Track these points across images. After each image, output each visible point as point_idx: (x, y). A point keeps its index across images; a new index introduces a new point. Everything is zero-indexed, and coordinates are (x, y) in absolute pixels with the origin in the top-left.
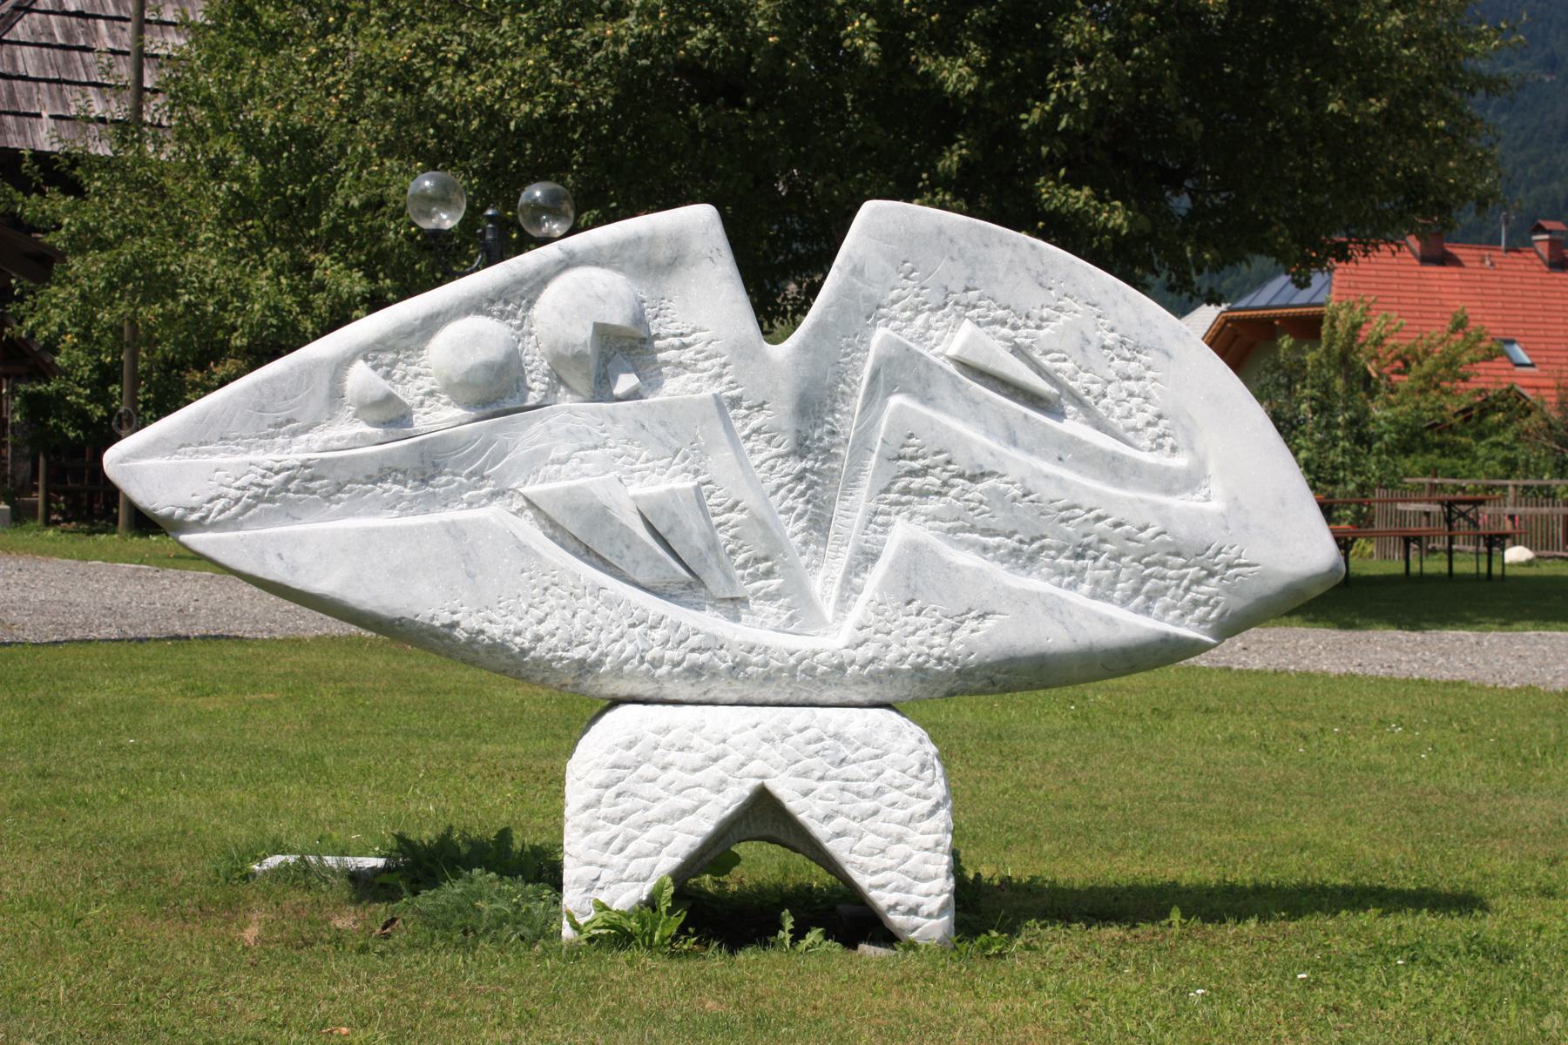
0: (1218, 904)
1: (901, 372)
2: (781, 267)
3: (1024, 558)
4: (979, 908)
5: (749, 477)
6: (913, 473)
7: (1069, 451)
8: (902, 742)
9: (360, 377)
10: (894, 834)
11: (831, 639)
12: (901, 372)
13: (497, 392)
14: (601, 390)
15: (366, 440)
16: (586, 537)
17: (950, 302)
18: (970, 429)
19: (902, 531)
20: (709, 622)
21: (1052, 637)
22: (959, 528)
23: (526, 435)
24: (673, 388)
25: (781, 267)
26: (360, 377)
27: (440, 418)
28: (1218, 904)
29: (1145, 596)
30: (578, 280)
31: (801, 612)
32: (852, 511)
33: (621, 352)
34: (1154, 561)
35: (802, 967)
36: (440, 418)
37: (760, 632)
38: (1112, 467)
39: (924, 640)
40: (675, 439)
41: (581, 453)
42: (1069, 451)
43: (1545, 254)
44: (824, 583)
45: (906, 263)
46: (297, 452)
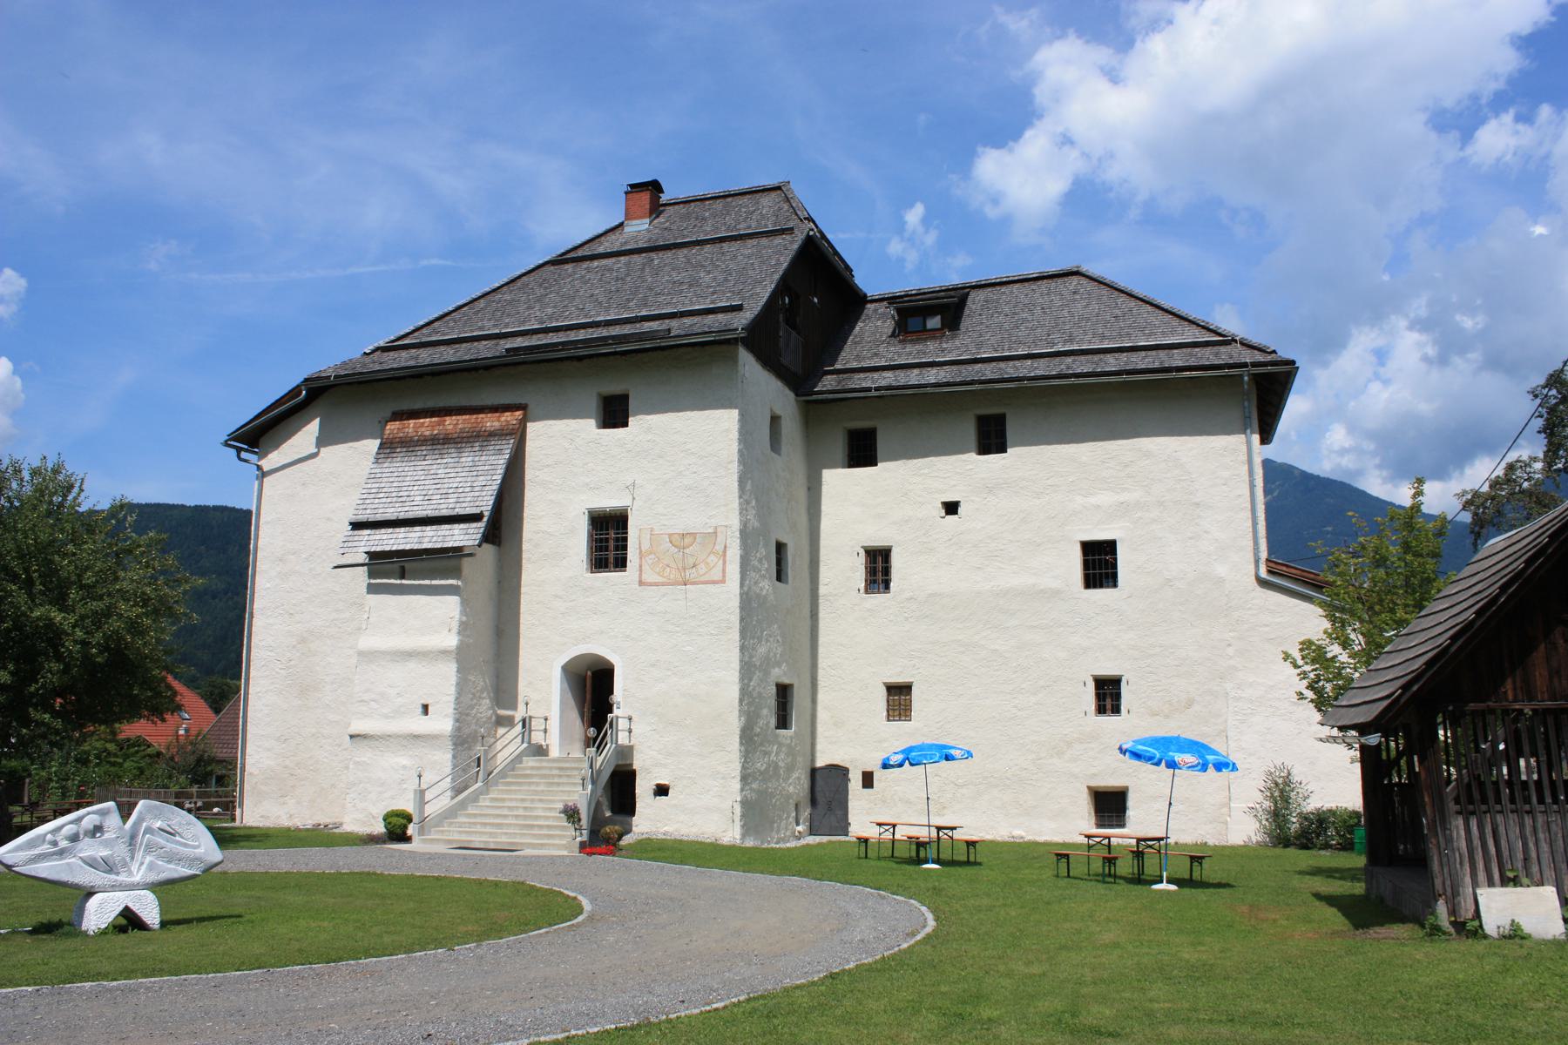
0: (201, 920)
1: (149, 830)
2: (125, 811)
3: (169, 862)
4: (163, 924)
5: (121, 850)
6: (149, 848)
7: (178, 843)
8: (149, 896)
9: (49, 837)
10: (150, 912)
11: (137, 878)
12: (149, 830)
13: (74, 838)
14: (93, 836)
15: (1514, 683)
16: (91, 863)
17: (157, 817)
18: (160, 840)
19: (148, 859)
20: (113, 877)
21: (175, 875)
22: (159, 857)
23: (80, 845)
24: (106, 836)
25: (125, 811)
26: (49, 837)
27: (64, 844)
28: (201, 920)
29: (190, 867)
30: (88, 816)
31: (130, 873)
32: (139, 855)
33: (98, 829)
34: (192, 861)
35: (136, 934)
36: (64, 844)
37: (123, 878)
38: (185, 845)
39: (153, 877)
40: (107, 844)
41: (89, 848)
42: (178, 843)
43: (1458, 519)
44: (134, 868)
45: (149, 809)
46: (37, 851)
